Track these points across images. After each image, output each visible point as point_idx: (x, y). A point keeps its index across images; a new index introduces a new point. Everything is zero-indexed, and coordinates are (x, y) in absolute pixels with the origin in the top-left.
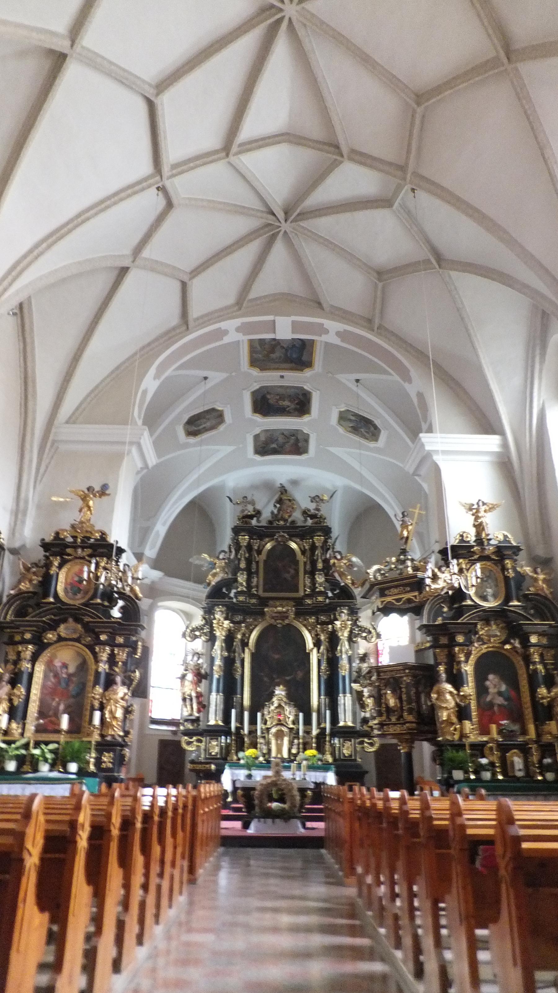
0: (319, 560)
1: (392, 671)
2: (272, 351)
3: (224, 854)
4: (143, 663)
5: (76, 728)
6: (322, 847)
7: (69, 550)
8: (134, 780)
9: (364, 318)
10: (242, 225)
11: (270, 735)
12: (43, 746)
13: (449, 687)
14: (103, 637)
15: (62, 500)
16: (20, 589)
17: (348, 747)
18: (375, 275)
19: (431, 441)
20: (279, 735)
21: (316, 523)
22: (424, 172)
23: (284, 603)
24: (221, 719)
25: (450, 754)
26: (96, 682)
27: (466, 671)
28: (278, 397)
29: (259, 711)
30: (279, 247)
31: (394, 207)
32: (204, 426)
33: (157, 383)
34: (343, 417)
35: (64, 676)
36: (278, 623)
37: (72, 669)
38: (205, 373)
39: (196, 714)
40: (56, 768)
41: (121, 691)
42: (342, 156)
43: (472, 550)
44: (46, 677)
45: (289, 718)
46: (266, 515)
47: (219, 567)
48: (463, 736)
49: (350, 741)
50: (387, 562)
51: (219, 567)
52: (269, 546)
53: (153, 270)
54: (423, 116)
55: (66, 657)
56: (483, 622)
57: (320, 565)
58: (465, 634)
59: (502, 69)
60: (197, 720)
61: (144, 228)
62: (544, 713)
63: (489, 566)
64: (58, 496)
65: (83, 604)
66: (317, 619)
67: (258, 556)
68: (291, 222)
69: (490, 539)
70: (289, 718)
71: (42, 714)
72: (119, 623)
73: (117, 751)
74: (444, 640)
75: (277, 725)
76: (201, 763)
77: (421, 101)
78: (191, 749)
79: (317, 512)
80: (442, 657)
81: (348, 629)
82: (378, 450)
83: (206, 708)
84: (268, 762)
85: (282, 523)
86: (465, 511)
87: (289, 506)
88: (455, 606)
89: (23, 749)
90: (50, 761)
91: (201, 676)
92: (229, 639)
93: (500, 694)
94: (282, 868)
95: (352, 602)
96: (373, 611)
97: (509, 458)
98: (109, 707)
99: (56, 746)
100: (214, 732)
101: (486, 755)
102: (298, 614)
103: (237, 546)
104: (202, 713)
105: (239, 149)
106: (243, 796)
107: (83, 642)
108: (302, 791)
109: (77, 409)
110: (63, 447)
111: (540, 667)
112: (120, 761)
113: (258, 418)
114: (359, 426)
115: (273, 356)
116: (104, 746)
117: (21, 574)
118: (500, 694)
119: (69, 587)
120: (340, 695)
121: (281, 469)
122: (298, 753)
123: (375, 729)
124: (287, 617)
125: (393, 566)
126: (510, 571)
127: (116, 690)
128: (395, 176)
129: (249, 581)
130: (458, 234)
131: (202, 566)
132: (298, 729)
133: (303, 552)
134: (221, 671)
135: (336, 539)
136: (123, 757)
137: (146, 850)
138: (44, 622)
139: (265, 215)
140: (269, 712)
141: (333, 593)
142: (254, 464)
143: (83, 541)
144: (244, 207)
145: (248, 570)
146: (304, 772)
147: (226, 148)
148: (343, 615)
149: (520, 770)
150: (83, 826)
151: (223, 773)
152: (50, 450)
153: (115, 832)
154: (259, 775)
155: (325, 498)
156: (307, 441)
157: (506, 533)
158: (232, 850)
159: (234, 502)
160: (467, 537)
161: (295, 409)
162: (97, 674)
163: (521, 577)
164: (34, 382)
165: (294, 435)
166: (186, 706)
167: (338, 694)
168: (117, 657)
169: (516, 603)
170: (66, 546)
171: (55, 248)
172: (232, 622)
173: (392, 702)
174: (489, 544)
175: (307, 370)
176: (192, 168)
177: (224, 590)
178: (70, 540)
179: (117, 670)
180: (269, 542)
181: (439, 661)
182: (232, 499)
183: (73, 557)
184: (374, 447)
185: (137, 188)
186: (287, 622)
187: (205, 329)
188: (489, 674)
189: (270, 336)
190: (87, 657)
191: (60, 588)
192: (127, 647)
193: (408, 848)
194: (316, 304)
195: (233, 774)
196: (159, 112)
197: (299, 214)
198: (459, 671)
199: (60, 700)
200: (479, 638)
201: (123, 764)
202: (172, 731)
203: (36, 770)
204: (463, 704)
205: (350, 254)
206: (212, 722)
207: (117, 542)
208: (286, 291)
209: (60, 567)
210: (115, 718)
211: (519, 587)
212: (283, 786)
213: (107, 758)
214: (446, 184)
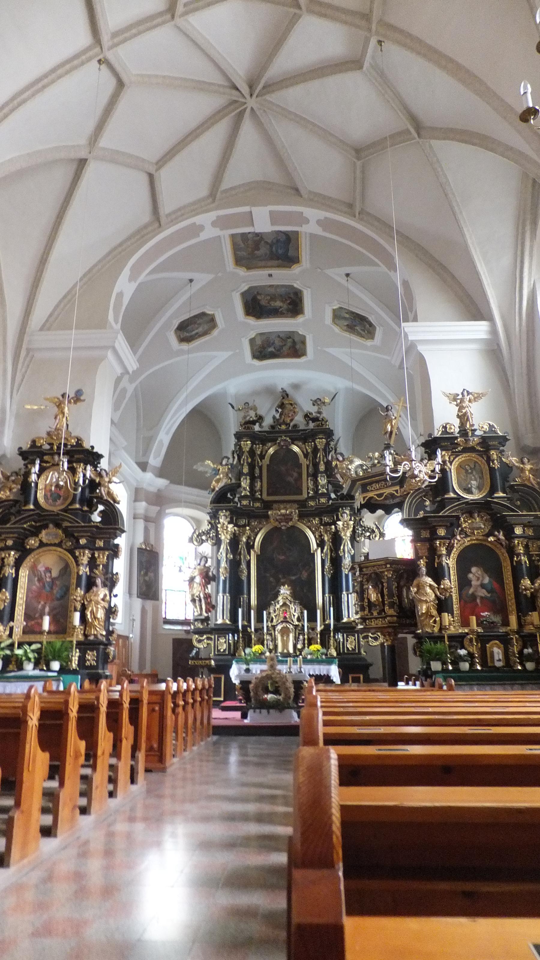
1: (374, 566)
2: (257, 247)
9: (345, 203)
10: (205, 104)
11: (276, 632)
12: (26, 647)
13: (429, 580)
14: (83, 541)
15: (36, 407)
17: (351, 642)
18: (353, 153)
20: (285, 632)
21: (318, 426)
22: (392, 19)
24: (229, 618)
26: (78, 585)
27: (447, 564)
28: (269, 298)
29: (265, 609)
30: (247, 127)
31: (364, 68)
32: (196, 331)
33: (133, 286)
34: (337, 315)
35: (48, 580)
36: (282, 526)
37: (55, 573)
38: (190, 275)
40: (40, 667)
43: (456, 442)
45: (294, 616)
46: (268, 422)
47: (223, 473)
49: (354, 636)
50: (369, 457)
51: (223, 473)
52: (271, 451)
53: (114, 161)
55: (48, 561)
57: (322, 468)
60: (207, 619)
62: (527, 604)
63: (468, 456)
65: (61, 510)
67: (261, 461)
69: (475, 430)
71: (28, 617)
72: (97, 527)
73: (101, 650)
75: (282, 622)
79: (318, 415)
80: (424, 552)
81: (351, 529)
82: (375, 349)
85: (283, 427)
87: (291, 410)
88: (438, 499)
89: (9, 649)
91: (208, 578)
92: (234, 542)
93: (483, 586)
97: (498, 345)
98: (90, 609)
99: (39, 646)
100: (221, 631)
102: (302, 516)
103: (239, 452)
105: (184, 10)
107: (64, 547)
109: (51, 315)
111: (524, 559)
112: (105, 659)
113: (251, 321)
114: (354, 323)
116: (85, 646)
118: (483, 586)
120: (344, 593)
121: (281, 373)
122: (304, 647)
124: (291, 520)
125: (376, 461)
126: (496, 461)
127: (97, 591)
130: (436, 94)
131: (206, 472)
132: (303, 626)
133: (306, 456)
134: (227, 572)
135: (338, 440)
138: (24, 529)
139: (228, 90)
140: (275, 611)
141: (336, 495)
149: (499, 660)
154: (257, 669)
156: (304, 342)
157: (491, 423)
160: (451, 428)
161: (288, 310)
162: (79, 577)
163: (507, 468)
165: (290, 338)
167: (342, 591)
168: (98, 560)
169: (501, 494)
172: (236, 525)
173: (373, 596)
175: (295, 266)
177: (229, 495)
180: (271, 447)
182: (233, 404)
183: (51, 464)
186: (290, 524)
187: (179, 224)
188: (472, 566)
190: (69, 562)
191: (40, 496)
194: (294, 191)
197: (264, 87)
198: (440, 564)
199: (45, 603)
200: (462, 530)
202: (185, 630)
203: (20, 667)
204: (443, 597)
205: (324, 130)
206: (220, 621)
210: (95, 618)
211: (505, 478)
212: (277, 679)
213: (91, 657)
214: (415, 31)
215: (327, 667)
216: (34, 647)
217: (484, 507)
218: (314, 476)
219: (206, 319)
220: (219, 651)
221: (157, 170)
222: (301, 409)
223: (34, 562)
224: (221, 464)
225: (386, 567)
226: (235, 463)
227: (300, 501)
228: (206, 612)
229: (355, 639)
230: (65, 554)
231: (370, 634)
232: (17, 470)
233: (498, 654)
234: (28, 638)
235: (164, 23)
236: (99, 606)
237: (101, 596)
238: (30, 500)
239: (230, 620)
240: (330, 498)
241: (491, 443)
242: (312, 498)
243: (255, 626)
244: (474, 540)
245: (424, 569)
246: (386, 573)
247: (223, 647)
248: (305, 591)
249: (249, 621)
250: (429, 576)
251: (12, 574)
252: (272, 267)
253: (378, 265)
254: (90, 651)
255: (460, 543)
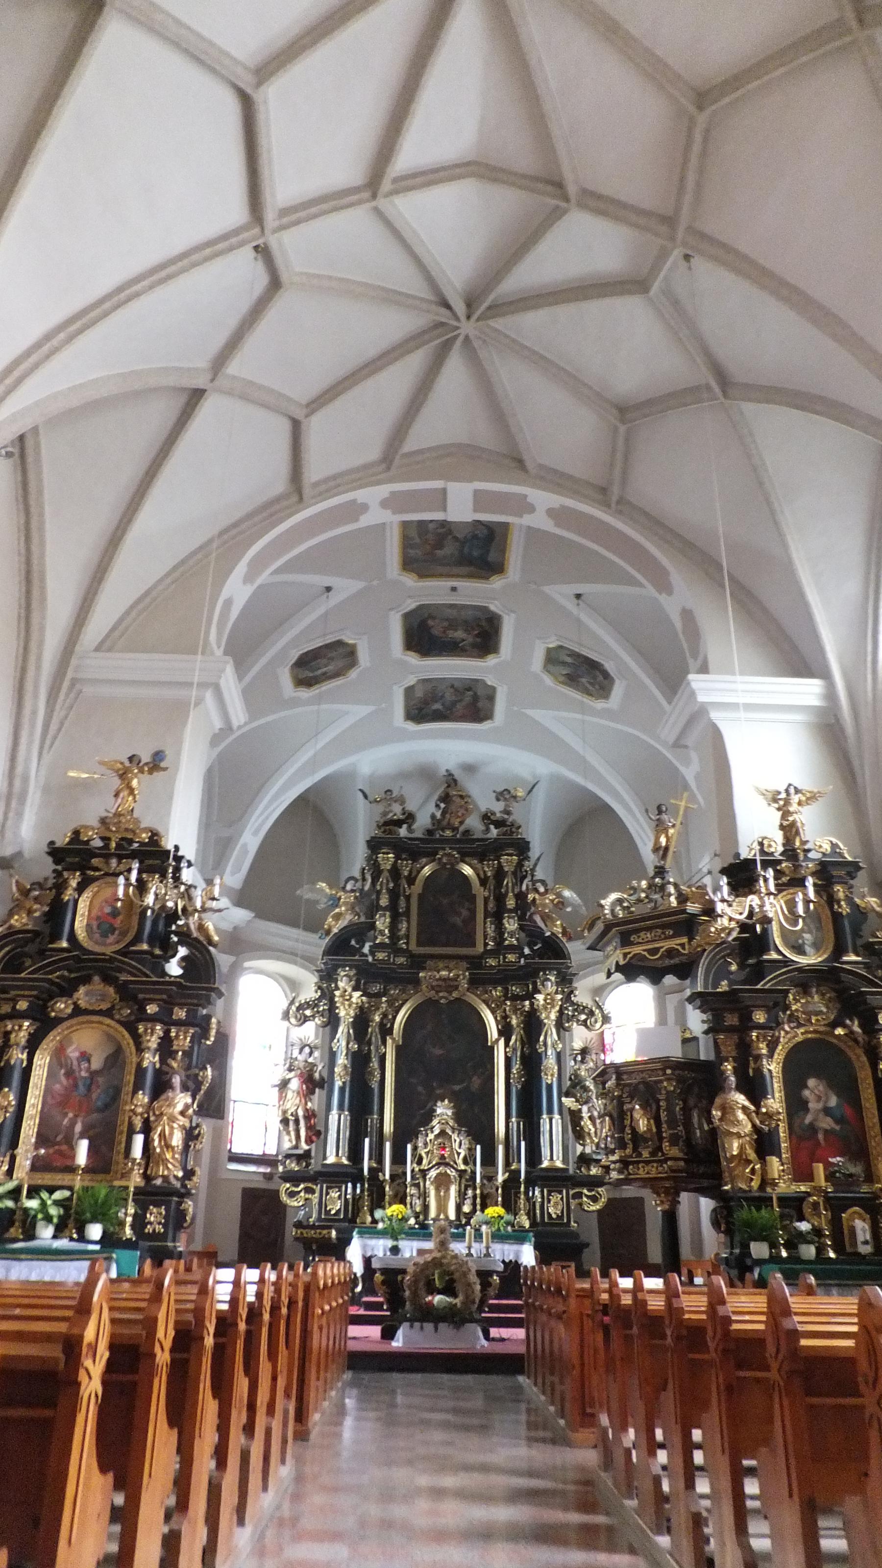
0: (508, 892)
1: (642, 1072)
2: (439, 545)
3: (353, 1384)
4: (219, 1053)
5: (101, 1163)
6: (521, 1372)
7: (95, 861)
8: (202, 1255)
9: (588, 483)
10: (397, 324)
11: (428, 1183)
12: (44, 1195)
13: (741, 1099)
14: (151, 1009)
16: (11, 927)
17: (556, 1204)
18: (614, 411)
19: (704, 687)
20: (442, 1182)
22: (711, 226)
23: (452, 964)
25: (744, 1213)
26: (138, 1086)
27: (770, 1071)
29: (410, 1141)
30: (455, 369)
32: (324, 670)
34: (552, 659)
35: (84, 1074)
37: (97, 1063)
38: (327, 581)
39: (305, 1147)
41: (182, 1100)
42: (567, 200)
44: (51, 1075)
45: (459, 1154)
46: (423, 821)
47: (345, 903)
48: (765, 1182)
49: (560, 1192)
52: (427, 871)
53: (244, 397)
54: (707, 131)
55: (87, 1042)
56: (798, 989)
57: (511, 903)
58: (768, 1010)
59: (848, 39)
60: (307, 1155)
61: (232, 322)
64: (79, 769)
66: (506, 990)
68: (478, 320)
69: (809, 850)
70: (459, 1154)
71: (42, 1139)
73: (173, 1206)
74: (732, 1020)
75: (438, 1164)
76: (313, 1227)
77: (704, 104)
78: (296, 1204)
79: (506, 816)
80: (729, 1048)
81: (557, 1008)
82: (608, 714)
83: (322, 1137)
84: (424, 1226)
85: (448, 833)
86: (765, 803)
87: (461, 807)
89: (11, 1199)
90: (55, 1220)
91: (312, 1083)
92: (361, 1022)
93: (827, 1111)
94: (456, 1411)
95: (562, 964)
96: (609, 970)
98: (159, 1129)
99: (67, 1193)
100: (333, 1177)
101: (807, 1216)
102: (475, 982)
104: (313, 1145)
105: (392, 187)
106: (383, 1282)
107: (117, 1017)
108: (484, 1275)
109: (114, 629)
110: (88, 690)
112: (177, 1221)
113: (413, 659)
115: (440, 553)
116: (148, 1196)
117: (14, 900)
118: (827, 1111)
119: (95, 924)
120: (545, 1116)
121: (449, 746)
122: (474, 1211)
123: (614, 1170)
124: (456, 988)
125: (643, 895)
126: (843, 903)
127: (173, 1098)
128: (656, 234)
129: (393, 927)
131: (317, 902)
132: (474, 1173)
133: (483, 882)
136: (182, 1214)
137: (222, 1389)
139: (434, 307)
140: (426, 1144)
141: (531, 949)
142: (404, 736)
143: (119, 846)
144: (400, 293)
145: (393, 907)
146: (487, 1243)
147: (373, 184)
148: (549, 984)
149: (866, 1243)
150: (93, 1348)
151: (349, 1244)
152: (67, 695)
153: (163, 1357)
154: (410, 1249)
155: (519, 794)
156: (491, 698)
157: (835, 841)
158: (366, 1377)
159: (371, 798)
160: (770, 846)
161: (474, 645)
162: (140, 1072)
163: (860, 914)
164: (42, 579)
165: (469, 689)
166: (288, 1133)
167: (540, 1114)
168: (175, 1042)
169: (853, 958)
170: (92, 853)
171: (82, 341)
173: (642, 1125)
174: (806, 858)
176: (315, 216)
177: (353, 942)
178: (98, 843)
179: (175, 1065)
181: (724, 1054)
184: (603, 709)
185: (221, 246)
186: (455, 994)
189: (438, 516)
190: (124, 1044)
192: (193, 1025)
193: (730, 1390)
194: (515, 462)
195: (364, 1247)
196: (261, 117)
197: (489, 308)
198: (759, 1071)
199: (76, 1116)
201: (182, 1227)
202: (264, 1174)
203: (30, 1234)
204: (766, 1129)
206: (331, 1159)
207: (177, 848)
208: (467, 441)
209: (81, 889)
210: (168, 1146)
211: (856, 933)
212: (453, 1268)
213: (155, 1217)
214: (743, 247)
215: (515, 1247)
216: (58, 1195)
217: (826, 977)
218: (498, 917)
219: (341, 650)
220: (328, 1212)
221: (307, 416)
222: (476, 807)
223: (61, 1042)
224: (344, 888)
225: (665, 1074)
226: (367, 888)
227: (474, 957)
228: (306, 1142)
229: (562, 1199)
230: (116, 1030)
231: (585, 1191)
232: (41, 881)
233: (864, 1231)
234: (48, 1179)
235: (360, 202)
236: (175, 1125)
237: (180, 1107)
238: (62, 931)
239: (349, 1159)
240: (522, 955)
241: (834, 873)
242: (494, 953)
243: (391, 1170)
244: (810, 1032)
245: (733, 1079)
246: (665, 1084)
247: (336, 1206)
248: (476, 1111)
249: (380, 1160)
250: (741, 1092)
251: (22, 1061)
252: (458, 576)
253: (641, 585)
254: (155, 1206)
255: (789, 1036)
